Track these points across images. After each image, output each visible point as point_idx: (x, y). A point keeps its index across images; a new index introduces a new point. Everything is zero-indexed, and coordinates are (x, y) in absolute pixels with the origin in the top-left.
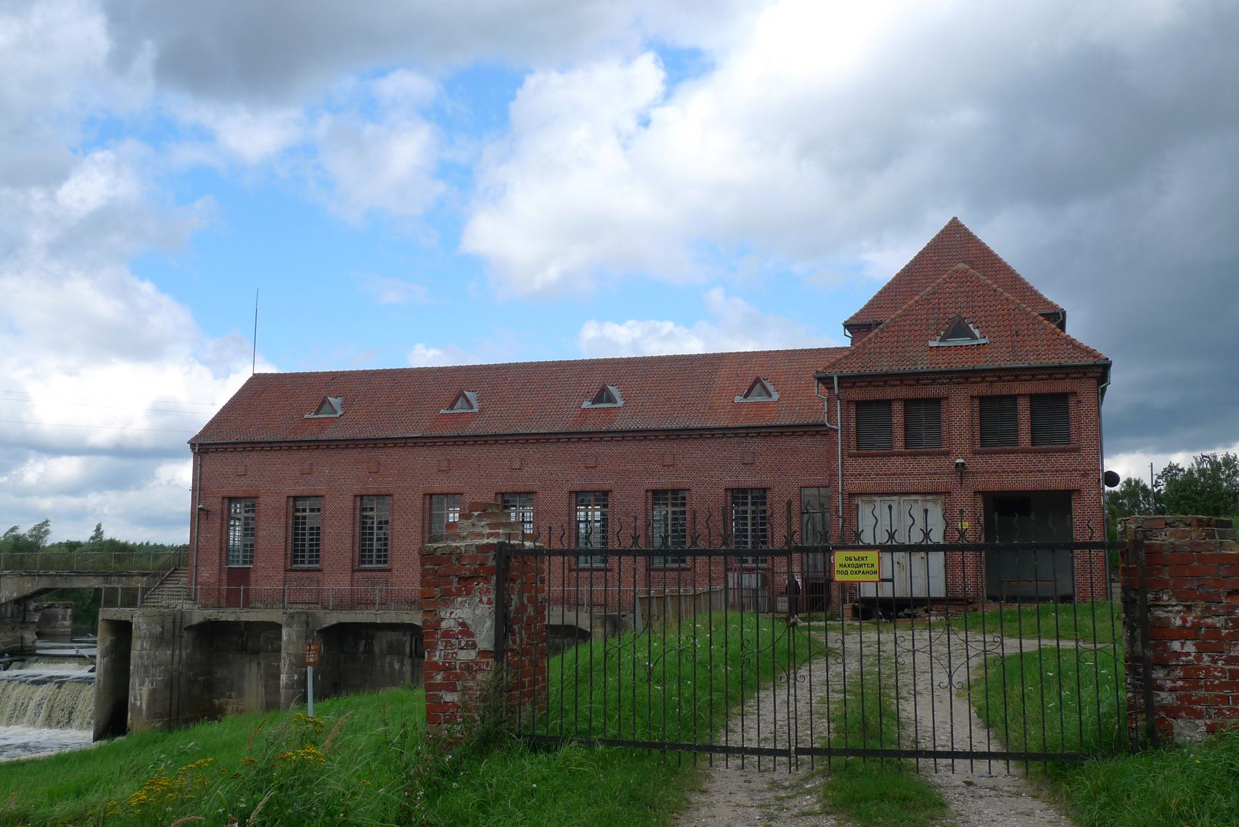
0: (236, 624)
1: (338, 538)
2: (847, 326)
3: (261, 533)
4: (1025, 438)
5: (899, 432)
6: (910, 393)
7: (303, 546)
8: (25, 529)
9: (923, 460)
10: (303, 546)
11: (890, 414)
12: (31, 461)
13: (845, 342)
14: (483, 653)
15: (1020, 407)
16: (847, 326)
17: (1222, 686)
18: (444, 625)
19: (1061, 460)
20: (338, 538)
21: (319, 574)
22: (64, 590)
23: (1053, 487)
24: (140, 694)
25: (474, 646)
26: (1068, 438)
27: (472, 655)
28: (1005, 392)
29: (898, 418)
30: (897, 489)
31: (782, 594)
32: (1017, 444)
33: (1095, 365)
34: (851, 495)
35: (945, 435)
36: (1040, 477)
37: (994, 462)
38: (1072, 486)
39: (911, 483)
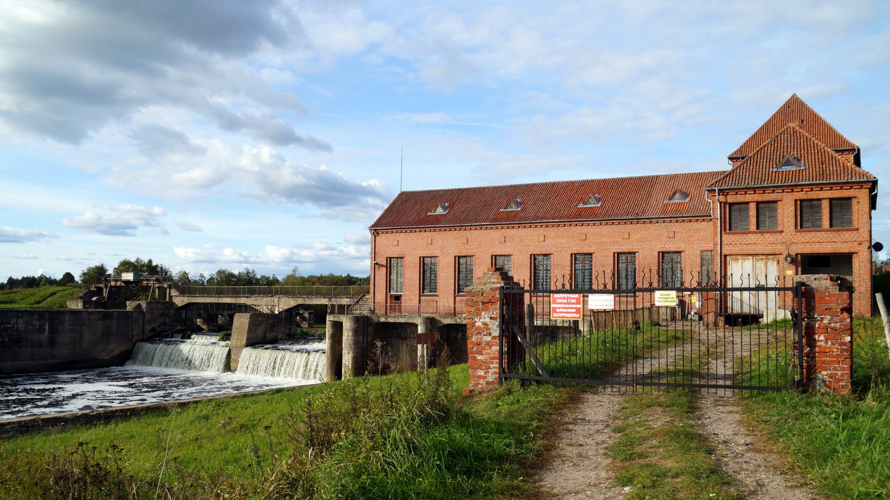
0: (395, 323)
1: (445, 278)
2: (731, 158)
3: (407, 276)
4: (826, 223)
5: (753, 220)
6: (758, 197)
7: (427, 280)
8: (290, 273)
9: (767, 236)
10: (427, 280)
11: (747, 210)
12: (105, 218)
13: (728, 167)
14: (494, 337)
15: (823, 206)
16: (731, 158)
17: (837, 356)
18: (477, 324)
19: (847, 235)
20: (445, 278)
21: (437, 298)
22: (309, 305)
23: (842, 251)
24: (347, 359)
25: (490, 334)
26: (850, 222)
27: (489, 338)
28: (815, 197)
29: (753, 212)
30: (752, 252)
31: (585, 303)
32: (821, 226)
33: (868, 182)
34: (725, 256)
35: (780, 222)
36: (835, 245)
37: (809, 236)
38: (853, 250)
39: (760, 249)
